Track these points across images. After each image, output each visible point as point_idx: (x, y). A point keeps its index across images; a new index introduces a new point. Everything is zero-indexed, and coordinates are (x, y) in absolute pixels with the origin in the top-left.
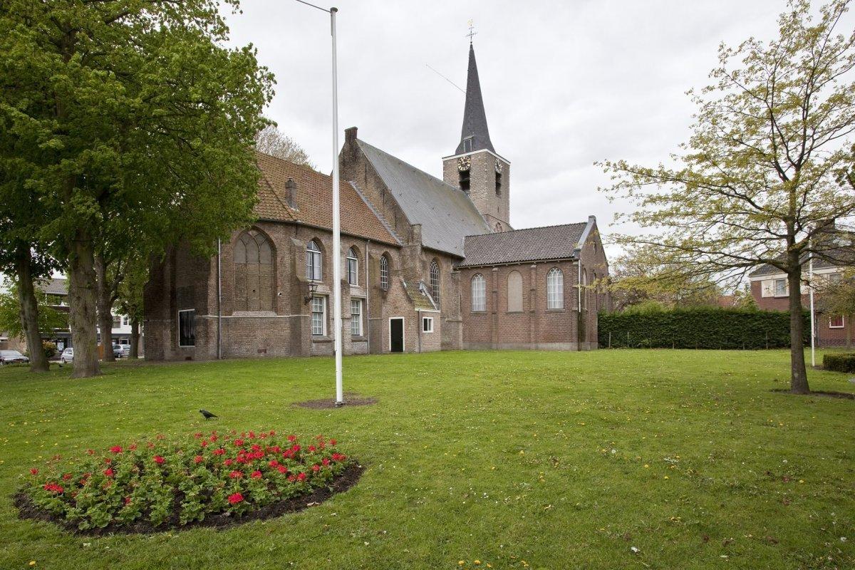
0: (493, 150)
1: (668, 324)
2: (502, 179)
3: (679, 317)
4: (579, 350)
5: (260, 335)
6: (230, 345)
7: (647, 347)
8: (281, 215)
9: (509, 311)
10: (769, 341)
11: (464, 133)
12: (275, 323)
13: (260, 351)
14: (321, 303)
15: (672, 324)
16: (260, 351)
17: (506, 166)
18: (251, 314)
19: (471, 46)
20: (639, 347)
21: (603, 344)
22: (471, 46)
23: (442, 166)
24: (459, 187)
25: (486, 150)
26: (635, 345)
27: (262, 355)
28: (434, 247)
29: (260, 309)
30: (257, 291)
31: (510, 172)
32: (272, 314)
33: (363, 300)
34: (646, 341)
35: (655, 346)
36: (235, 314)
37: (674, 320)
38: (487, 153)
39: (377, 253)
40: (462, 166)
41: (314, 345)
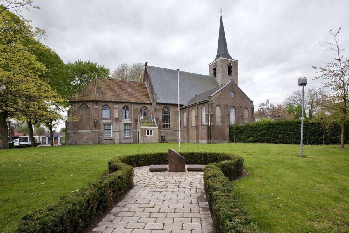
0: (230, 58)
1: (261, 130)
2: (233, 69)
3: (270, 126)
4: (209, 143)
5: (85, 137)
6: (77, 141)
7: (252, 142)
8: (91, 99)
9: (192, 126)
10: (325, 139)
11: (218, 51)
12: (89, 133)
13: (85, 142)
14: (111, 126)
15: (264, 130)
16: (85, 142)
17: (236, 63)
18: (83, 131)
19: (221, 16)
20: (248, 142)
21: (232, 140)
22: (221, 16)
23: (208, 68)
24: (213, 75)
25: (221, 58)
26: (246, 141)
27: (86, 143)
28: (168, 103)
29: (87, 129)
30: (86, 123)
31: (182, 71)
32: (89, 131)
33: (131, 124)
34: (251, 139)
35: (256, 141)
36: (79, 131)
37: (265, 128)
38: (221, 59)
39: (139, 107)
40: (214, 66)
41: (104, 140)
